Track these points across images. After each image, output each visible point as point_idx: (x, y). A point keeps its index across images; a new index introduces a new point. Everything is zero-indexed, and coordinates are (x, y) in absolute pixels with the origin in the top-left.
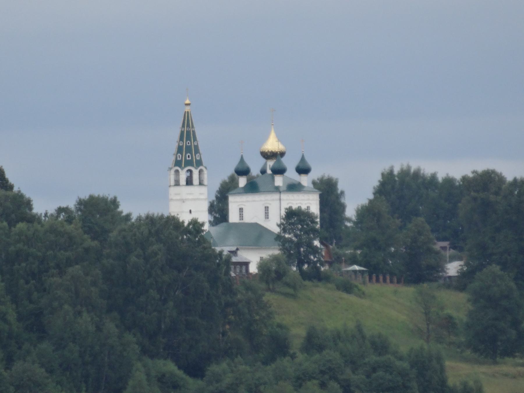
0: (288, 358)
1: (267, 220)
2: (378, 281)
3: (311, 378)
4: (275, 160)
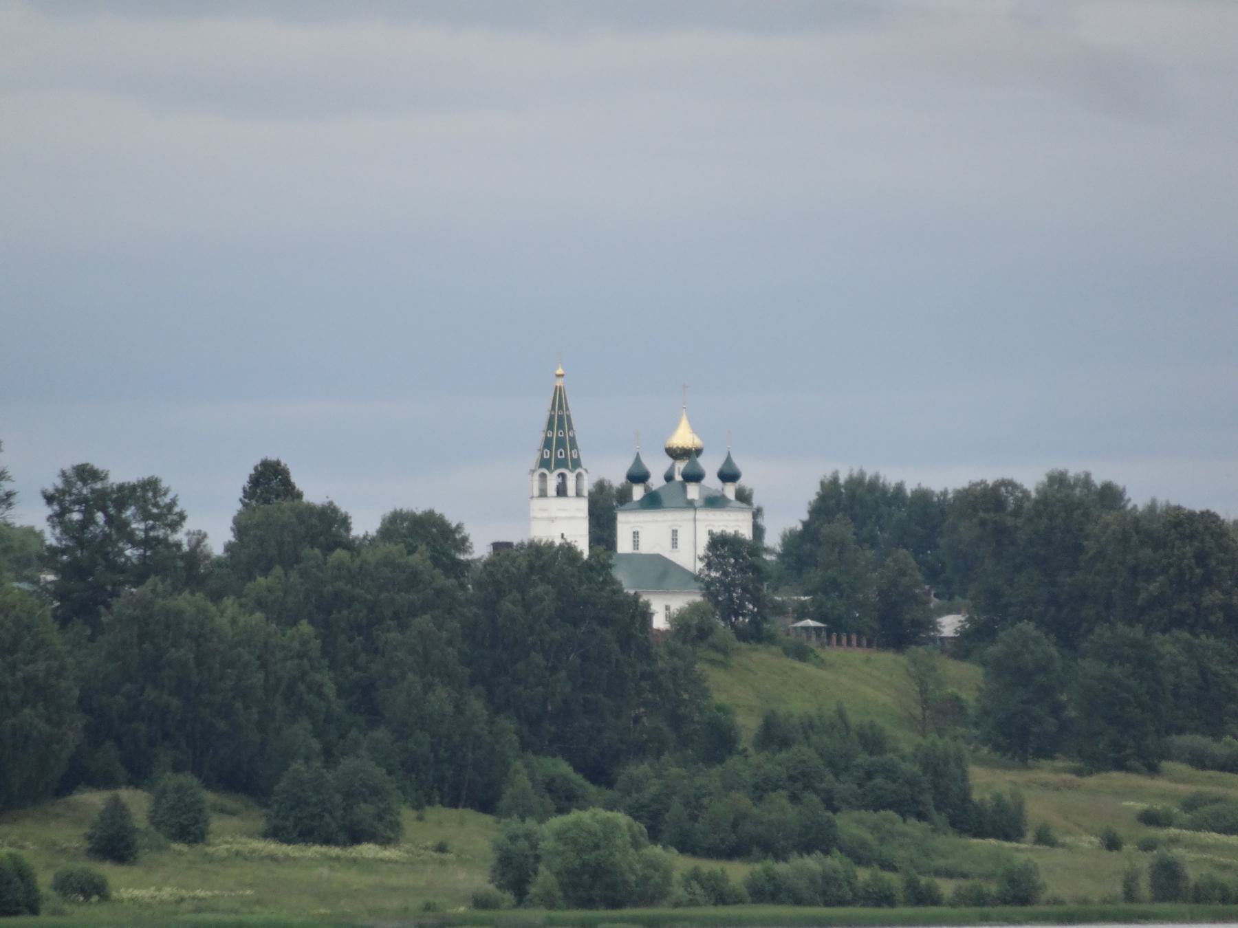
0: (736, 757)
1: (675, 549)
2: (839, 642)
3: (776, 788)
4: (687, 461)
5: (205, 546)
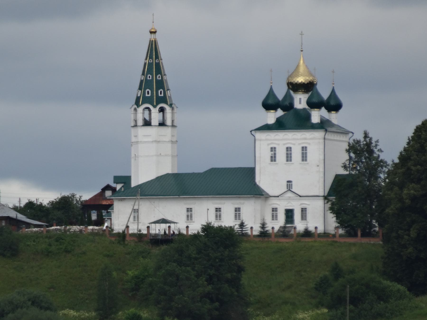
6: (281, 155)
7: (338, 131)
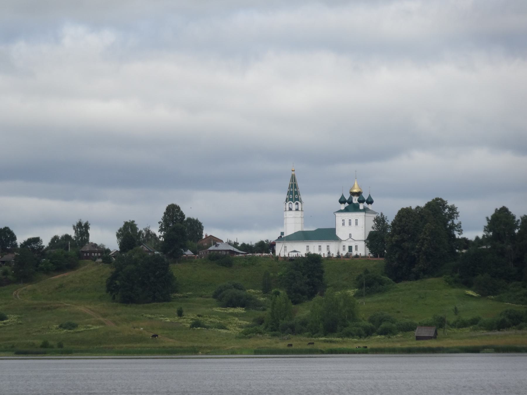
5: (151, 232)
6: (347, 223)
7: (371, 212)
